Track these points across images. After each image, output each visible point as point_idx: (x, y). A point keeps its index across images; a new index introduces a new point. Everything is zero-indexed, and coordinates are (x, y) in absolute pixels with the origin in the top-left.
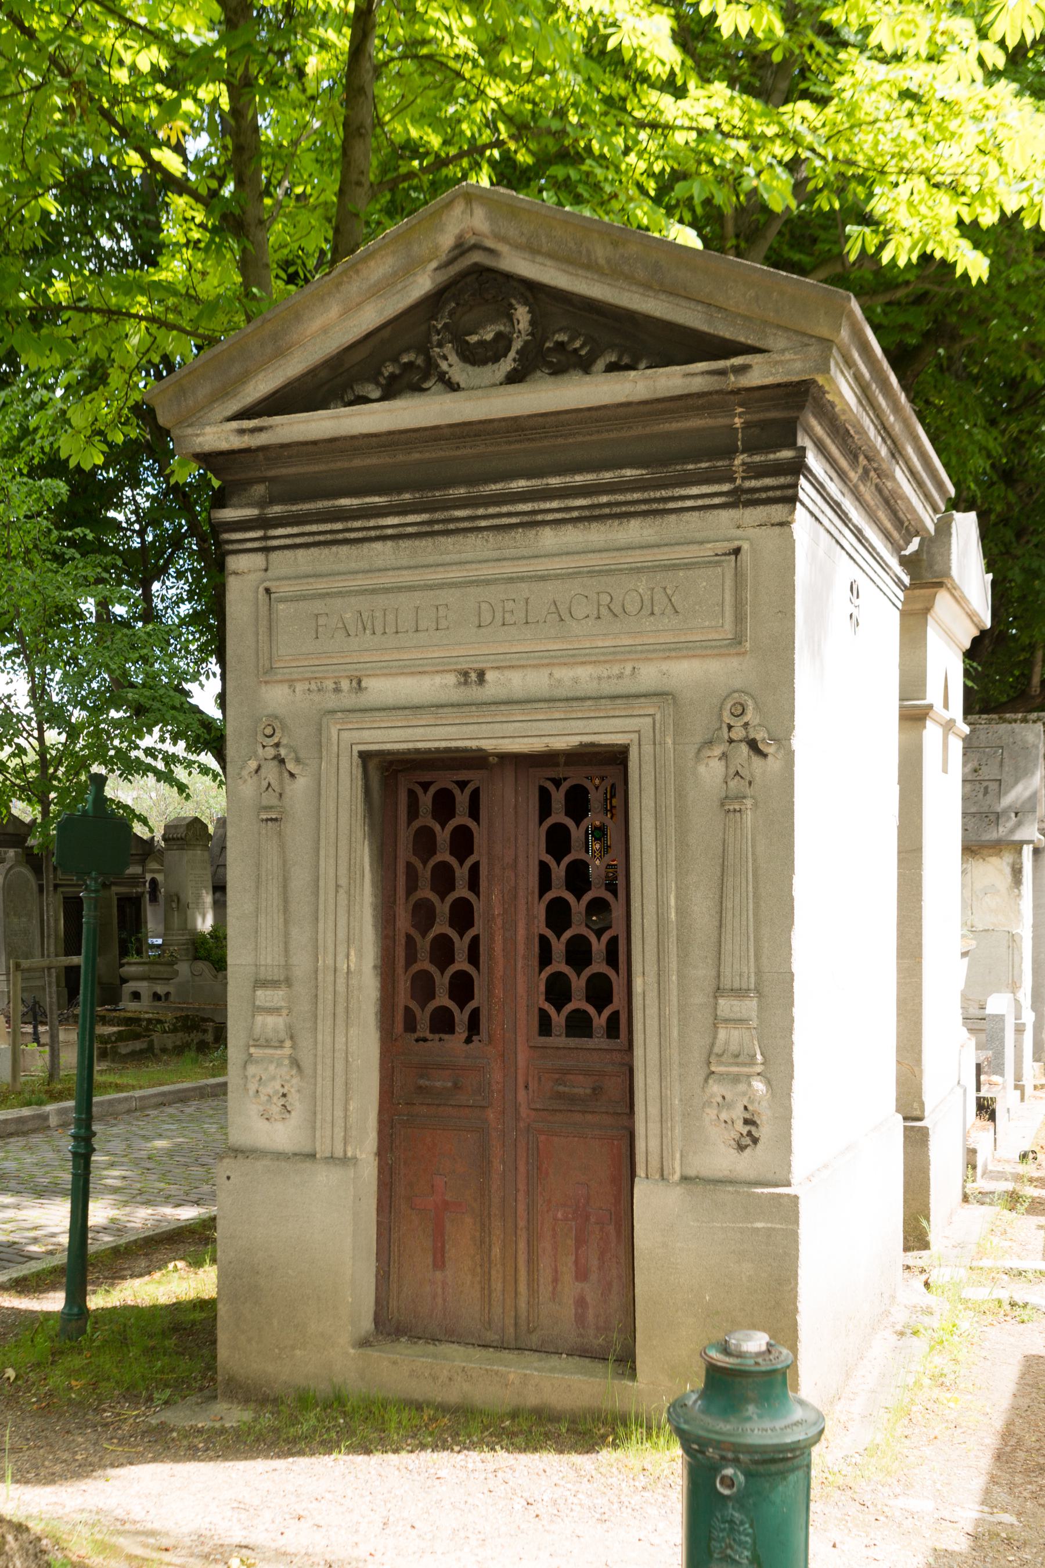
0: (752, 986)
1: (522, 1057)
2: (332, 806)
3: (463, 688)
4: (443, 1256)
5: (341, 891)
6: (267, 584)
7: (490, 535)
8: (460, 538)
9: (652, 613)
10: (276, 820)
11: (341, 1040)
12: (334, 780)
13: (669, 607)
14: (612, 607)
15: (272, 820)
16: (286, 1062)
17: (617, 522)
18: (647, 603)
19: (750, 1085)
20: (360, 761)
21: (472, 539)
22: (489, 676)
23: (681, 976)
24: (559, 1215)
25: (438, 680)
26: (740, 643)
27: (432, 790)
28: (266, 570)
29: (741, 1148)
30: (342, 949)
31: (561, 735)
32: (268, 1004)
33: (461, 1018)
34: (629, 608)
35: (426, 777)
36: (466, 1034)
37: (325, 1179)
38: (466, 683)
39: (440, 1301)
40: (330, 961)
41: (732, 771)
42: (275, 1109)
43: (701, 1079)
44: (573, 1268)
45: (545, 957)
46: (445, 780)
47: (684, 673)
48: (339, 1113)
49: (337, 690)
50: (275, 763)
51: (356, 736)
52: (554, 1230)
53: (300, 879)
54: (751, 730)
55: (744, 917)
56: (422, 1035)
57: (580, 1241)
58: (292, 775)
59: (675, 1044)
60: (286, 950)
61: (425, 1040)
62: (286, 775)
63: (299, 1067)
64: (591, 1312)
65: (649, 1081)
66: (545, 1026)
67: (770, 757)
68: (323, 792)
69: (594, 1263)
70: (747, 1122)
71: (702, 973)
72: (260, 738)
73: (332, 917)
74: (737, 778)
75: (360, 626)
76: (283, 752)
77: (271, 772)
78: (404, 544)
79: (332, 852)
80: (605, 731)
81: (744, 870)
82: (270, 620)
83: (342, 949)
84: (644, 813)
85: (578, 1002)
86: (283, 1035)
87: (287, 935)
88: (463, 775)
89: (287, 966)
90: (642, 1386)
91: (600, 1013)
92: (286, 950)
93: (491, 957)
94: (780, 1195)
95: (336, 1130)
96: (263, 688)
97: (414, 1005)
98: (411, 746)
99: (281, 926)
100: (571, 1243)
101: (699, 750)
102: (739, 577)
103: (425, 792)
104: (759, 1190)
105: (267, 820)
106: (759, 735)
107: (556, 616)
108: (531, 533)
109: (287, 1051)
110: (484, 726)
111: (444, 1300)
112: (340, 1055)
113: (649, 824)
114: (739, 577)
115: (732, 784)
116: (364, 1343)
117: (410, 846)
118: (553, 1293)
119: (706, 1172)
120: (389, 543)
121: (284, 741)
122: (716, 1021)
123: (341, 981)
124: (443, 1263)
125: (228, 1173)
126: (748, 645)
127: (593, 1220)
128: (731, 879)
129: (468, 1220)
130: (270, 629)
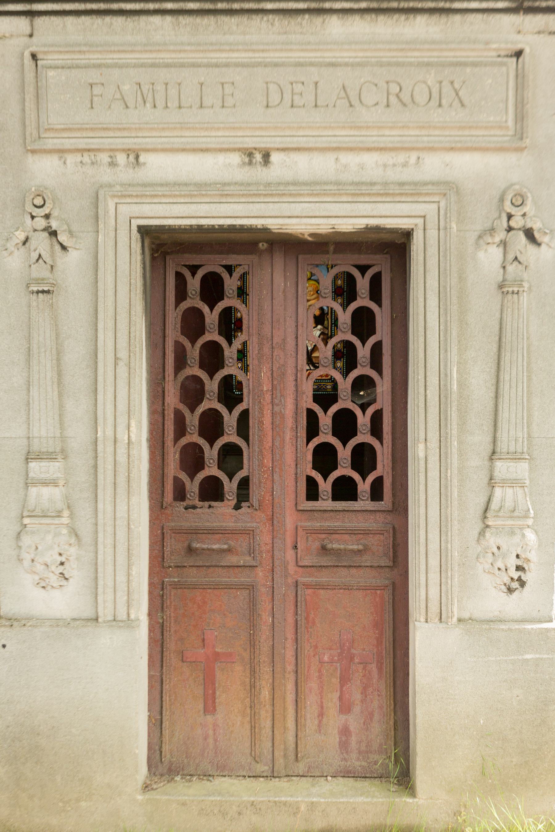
0: (525, 450)
1: (290, 520)
2: (110, 279)
3: (247, 168)
4: (214, 702)
5: (121, 364)
6: (33, 49)
7: (276, 19)
8: (244, 19)
9: (440, 105)
10: (48, 292)
11: (122, 508)
12: (111, 254)
13: (457, 100)
14: (402, 95)
15: (43, 292)
16: (65, 531)
17: (403, 17)
18: (435, 95)
19: (523, 535)
20: (139, 236)
21: (256, 20)
22: (275, 157)
23: (460, 443)
24: (326, 658)
25: (221, 158)
26: (521, 139)
27: (200, 274)
28: (31, 36)
29: (510, 590)
30: (122, 421)
31: (348, 217)
32: (43, 476)
33: (230, 487)
34: (417, 98)
35: (195, 260)
36: (235, 501)
37: (107, 640)
38: (250, 163)
39: (211, 741)
40: (110, 432)
41: (510, 257)
42: (54, 580)
43: (476, 533)
44: (338, 703)
45: (313, 429)
46: (212, 264)
47: (465, 166)
48: (121, 578)
49: (113, 164)
50: (46, 234)
51: (136, 210)
52: (320, 671)
53: (76, 352)
54: (528, 220)
55: (520, 389)
56: (191, 503)
57: (344, 679)
58: (64, 248)
59: (455, 503)
60: (61, 422)
61: (194, 507)
62: (57, 247)
63: (76, 535)
64: (353, 740)
65: (430, 536)
66: (312, 492)
67: (543, 246)
68: (101, 265)
69: (357, 696)
70: (519, 568)
71: (480, 439)
72: (29, 208)
73: (111, 389)
74: (516, 263)
75: (140, 99)
76: (54, 225)
77: (41, 243)
78: (184, 20)
79: (111, 324)
80: (390, 216)
81: (520, 346)
82: (37, 88)
83: (122, 421)
84: (429, 292)
85: (344, 469)
86: (60, 505)
87: (61, 407)
88: (231, 260)
89: (63, 438)
90: (421, 802)
91: (364, 479)
92: (61, 422)
93: (261, 429)
94: (547, 630)
95: (119, 594)
96: (30, 158)
97: (183, 476)
98: (194, 222)
99: (56, 398)
100: (336, 681)
101: (480, 237)
102: (521, 80)
103: (193, 274)
104: (529, 626)
105: (38, 292)
106: (536, 225)
107: (346, 101)
108: (318, 20)
109: (65, 520)
110: (271, 205)
111: (216, 740)
112: (121, 524)
113: (432, 302)
114: (521, 80)
115: (511, 268)
116: (146, 788)
117: (179, 326)
118: (319, 726)
119: (478, 614)
120: (168, 19)
121: (55, 213)
122: (491, 482)
123: (122, 451)
124: (215, 709)
125: (3, 642)
126: (528, 141)
127: (356, 660)
128: (508, 354)
129: (238, 668)
130: (37, 96)
